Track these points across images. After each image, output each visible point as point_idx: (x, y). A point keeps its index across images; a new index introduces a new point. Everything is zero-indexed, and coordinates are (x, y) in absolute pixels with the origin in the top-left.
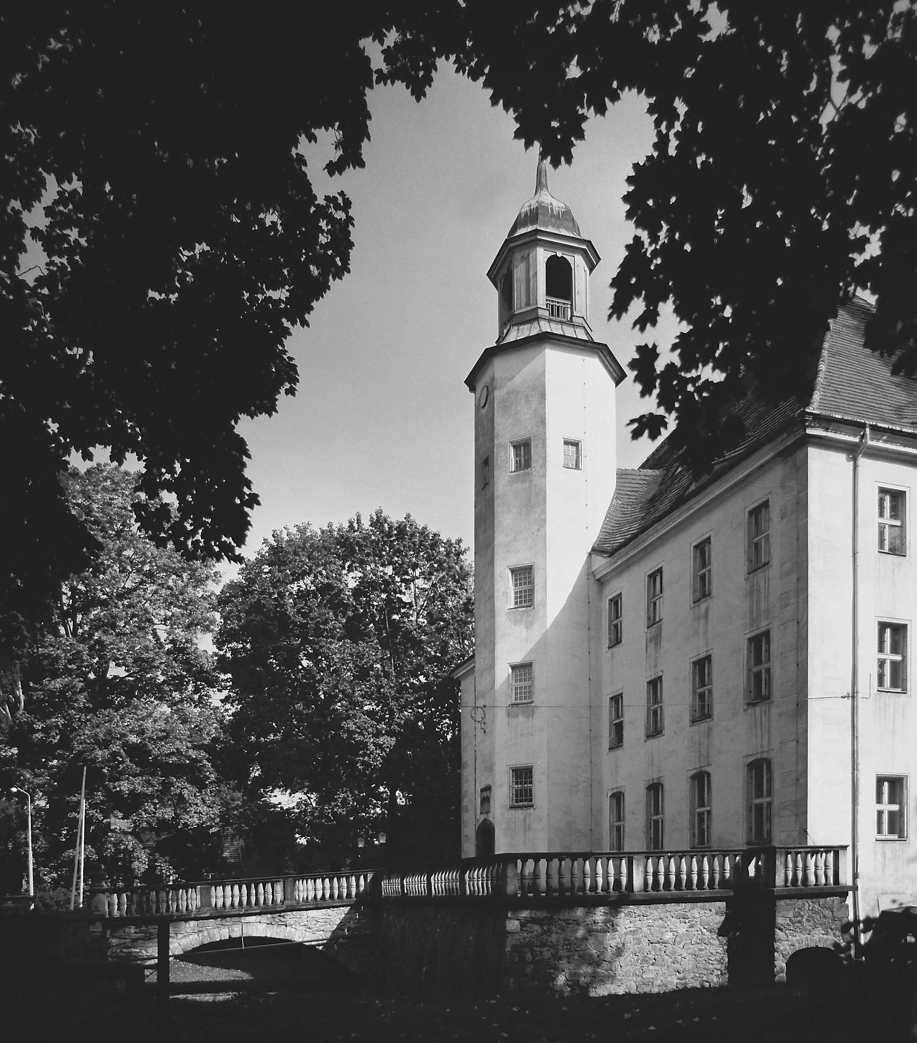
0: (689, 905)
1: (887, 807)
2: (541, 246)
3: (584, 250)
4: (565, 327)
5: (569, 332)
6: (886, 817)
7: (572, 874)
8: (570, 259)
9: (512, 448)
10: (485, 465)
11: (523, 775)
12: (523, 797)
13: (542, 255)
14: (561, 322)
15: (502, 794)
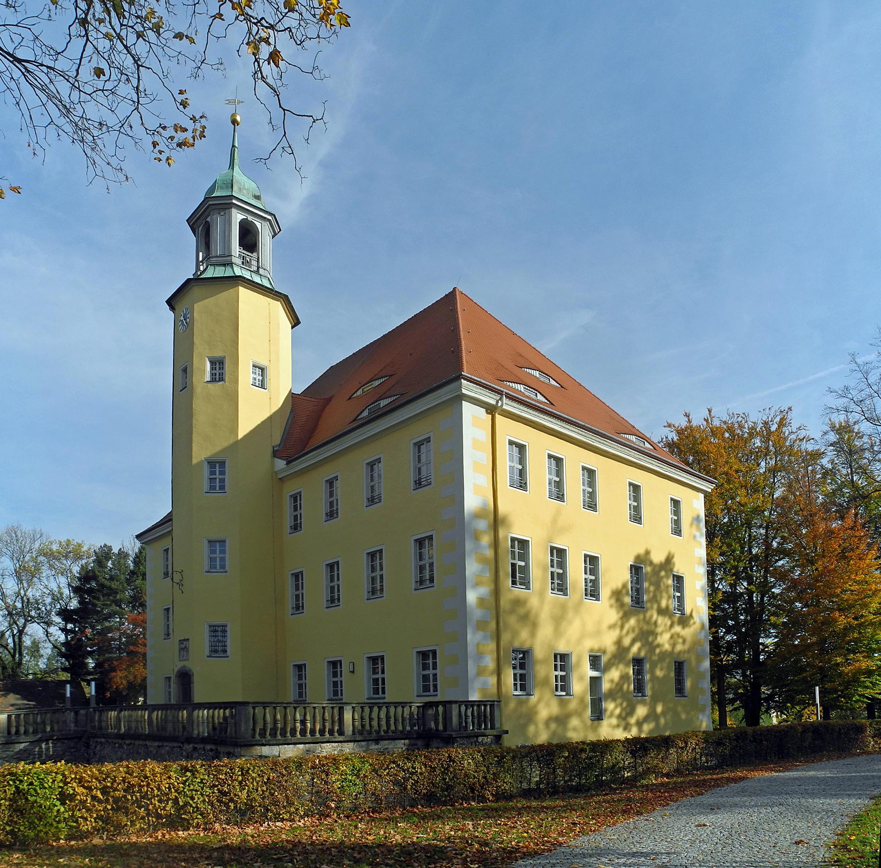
1: (431, 672)
3: (269, 220)
5: (257, 279)
8: (258, 225)
9: (208, 365)
10: (183, 374)
11: (218, 632)
12: (218, 649)
13: (237, 217)
15: (201, 642)
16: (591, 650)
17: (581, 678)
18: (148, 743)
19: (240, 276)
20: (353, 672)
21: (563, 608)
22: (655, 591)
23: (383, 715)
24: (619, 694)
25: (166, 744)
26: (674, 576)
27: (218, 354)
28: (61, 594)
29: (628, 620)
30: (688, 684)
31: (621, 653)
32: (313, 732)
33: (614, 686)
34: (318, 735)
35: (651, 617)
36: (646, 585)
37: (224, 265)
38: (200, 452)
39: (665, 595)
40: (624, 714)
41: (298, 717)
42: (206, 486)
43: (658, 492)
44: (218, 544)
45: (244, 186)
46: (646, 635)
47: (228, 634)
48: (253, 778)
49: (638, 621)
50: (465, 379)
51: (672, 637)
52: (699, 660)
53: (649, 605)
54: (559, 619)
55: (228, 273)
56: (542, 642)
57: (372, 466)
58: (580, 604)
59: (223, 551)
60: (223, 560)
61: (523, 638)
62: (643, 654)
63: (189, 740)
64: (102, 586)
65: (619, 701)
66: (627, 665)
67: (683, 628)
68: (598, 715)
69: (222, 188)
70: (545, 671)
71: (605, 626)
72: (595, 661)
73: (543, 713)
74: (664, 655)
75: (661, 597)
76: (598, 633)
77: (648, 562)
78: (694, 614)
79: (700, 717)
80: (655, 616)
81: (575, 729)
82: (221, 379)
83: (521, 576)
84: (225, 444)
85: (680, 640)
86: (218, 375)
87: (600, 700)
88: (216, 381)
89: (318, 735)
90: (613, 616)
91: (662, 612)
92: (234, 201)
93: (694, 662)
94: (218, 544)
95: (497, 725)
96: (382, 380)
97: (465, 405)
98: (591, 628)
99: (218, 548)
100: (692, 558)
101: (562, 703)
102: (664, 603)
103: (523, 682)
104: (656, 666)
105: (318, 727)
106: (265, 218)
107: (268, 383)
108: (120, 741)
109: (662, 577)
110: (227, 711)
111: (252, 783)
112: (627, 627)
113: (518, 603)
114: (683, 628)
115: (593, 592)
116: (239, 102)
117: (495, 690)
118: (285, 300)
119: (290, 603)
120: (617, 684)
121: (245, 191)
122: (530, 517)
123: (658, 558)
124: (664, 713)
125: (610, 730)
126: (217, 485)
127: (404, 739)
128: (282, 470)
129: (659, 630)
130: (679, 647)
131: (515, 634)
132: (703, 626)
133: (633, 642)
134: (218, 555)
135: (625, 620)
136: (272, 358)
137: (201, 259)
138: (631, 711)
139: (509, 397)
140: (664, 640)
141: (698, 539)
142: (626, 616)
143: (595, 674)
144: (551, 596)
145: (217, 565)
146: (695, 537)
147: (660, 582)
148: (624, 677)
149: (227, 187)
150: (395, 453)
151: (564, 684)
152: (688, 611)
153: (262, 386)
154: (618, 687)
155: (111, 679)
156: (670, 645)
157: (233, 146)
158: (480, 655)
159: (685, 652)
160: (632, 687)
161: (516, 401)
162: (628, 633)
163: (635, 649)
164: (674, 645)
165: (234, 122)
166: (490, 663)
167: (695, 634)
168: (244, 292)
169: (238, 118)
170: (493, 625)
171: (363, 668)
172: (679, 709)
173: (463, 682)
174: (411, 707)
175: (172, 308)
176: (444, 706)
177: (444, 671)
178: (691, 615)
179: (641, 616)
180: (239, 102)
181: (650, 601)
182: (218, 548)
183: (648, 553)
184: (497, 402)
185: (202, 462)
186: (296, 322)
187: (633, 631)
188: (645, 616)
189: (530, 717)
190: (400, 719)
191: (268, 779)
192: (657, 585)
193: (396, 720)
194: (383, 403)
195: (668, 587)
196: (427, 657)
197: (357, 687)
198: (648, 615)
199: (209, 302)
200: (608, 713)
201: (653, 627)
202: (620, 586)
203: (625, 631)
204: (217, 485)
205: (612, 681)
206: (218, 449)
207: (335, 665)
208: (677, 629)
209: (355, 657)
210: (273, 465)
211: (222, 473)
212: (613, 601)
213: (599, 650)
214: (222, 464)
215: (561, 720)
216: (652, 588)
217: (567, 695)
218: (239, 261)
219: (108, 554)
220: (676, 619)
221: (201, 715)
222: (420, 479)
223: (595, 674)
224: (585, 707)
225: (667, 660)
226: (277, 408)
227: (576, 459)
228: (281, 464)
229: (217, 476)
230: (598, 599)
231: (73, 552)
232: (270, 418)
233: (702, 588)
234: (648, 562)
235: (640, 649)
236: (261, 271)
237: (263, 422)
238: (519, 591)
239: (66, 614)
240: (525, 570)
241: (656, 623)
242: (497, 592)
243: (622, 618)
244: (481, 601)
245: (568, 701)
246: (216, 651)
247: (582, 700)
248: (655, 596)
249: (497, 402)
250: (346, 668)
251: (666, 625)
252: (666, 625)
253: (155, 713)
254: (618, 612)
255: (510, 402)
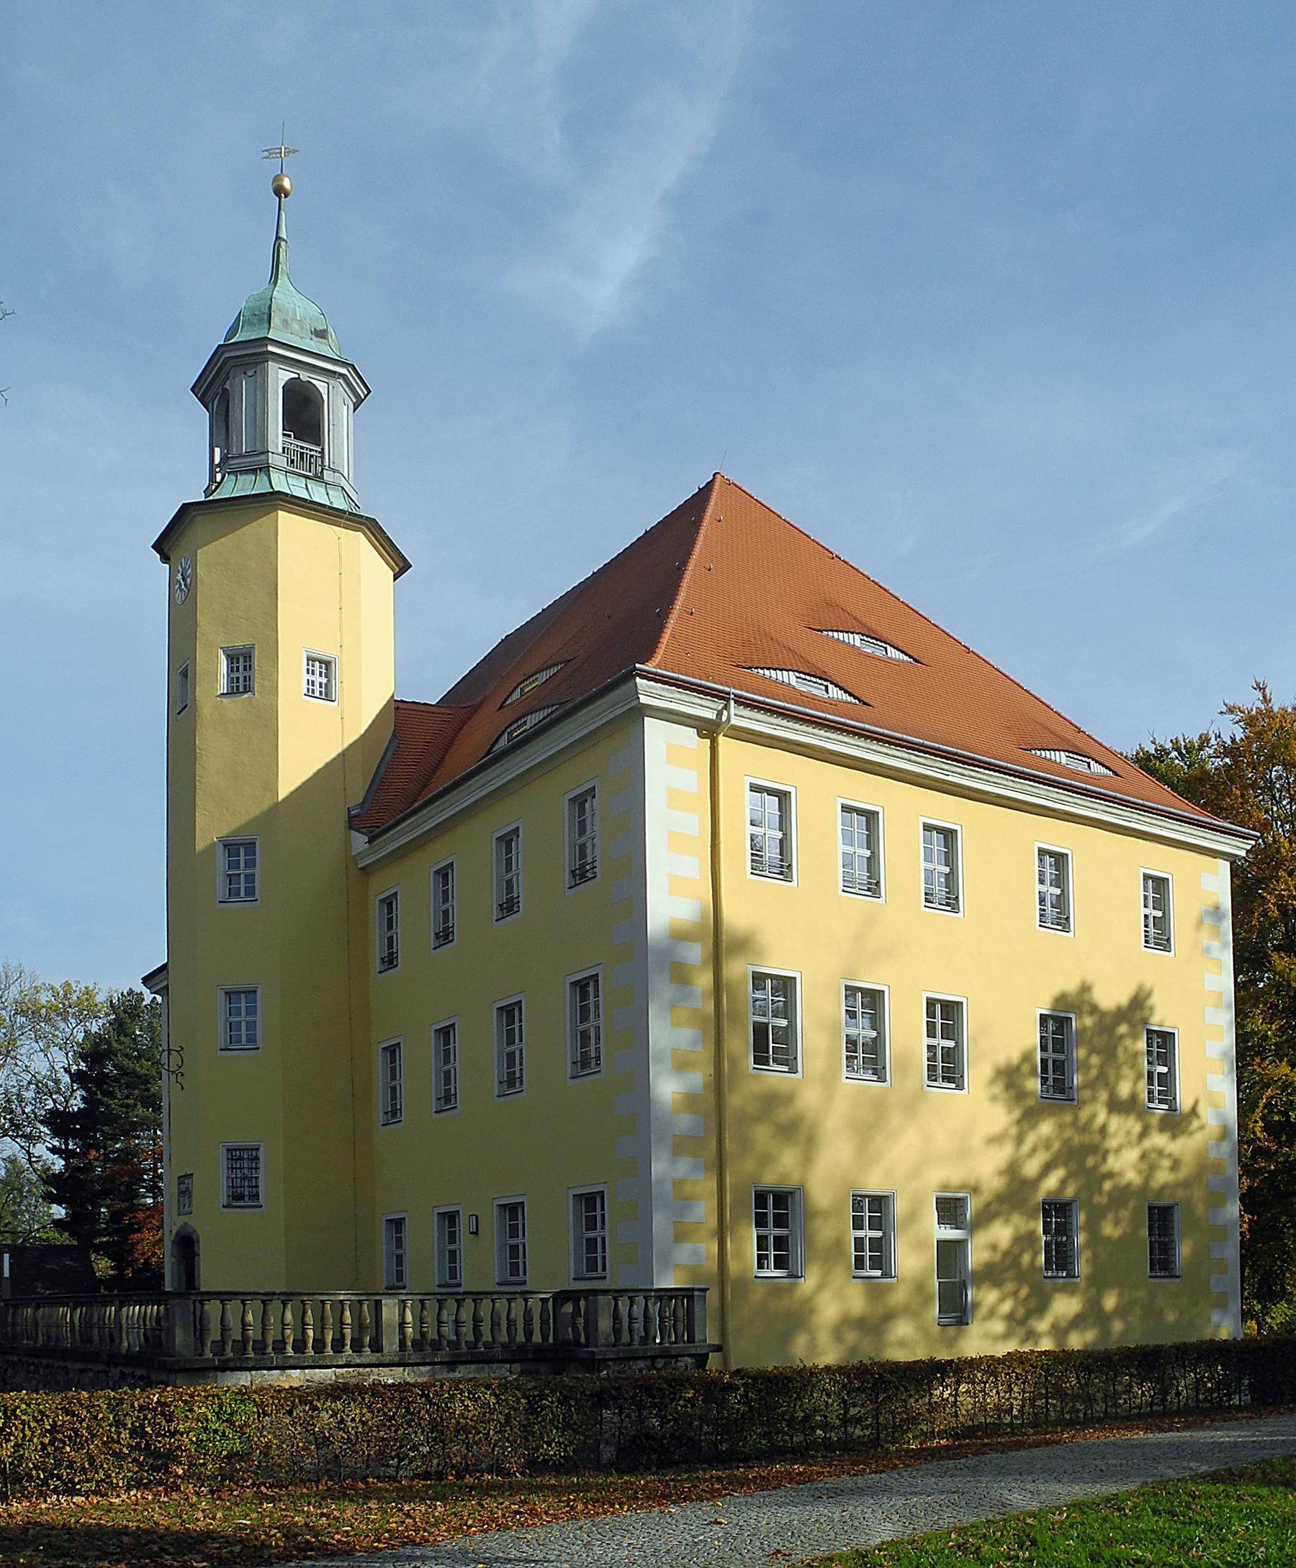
0: (386, 1370)
2: (273, 360)
3: (341, 375)
4: (311, 484)
5: (318, 494)
6: (600, 1268)
7: (439, 1322)
8: (322, 387)
10: (182, 676)
11: (243, 1159)
12: (242, 1193)
13: (279, 376)
14: (306, 477)
15: (213, 1181)
16: (945, 1187)
17: (920, 1245)
18: (69, 1364)
19: (279, 492)
20: (476, 1233)
21: (879, 1107)
22: (1102, 1067)
23: (466, 1315)
24: (1011, 1274)
25: (90, 1366)
26: (1149, 1032)
27: (240, 642)
28: (57, 1082)
29: (1034, 1125)
30: (1184, 1250)
31: (1015, 1192)
32: (319, 1345)
33: (998, 1257)
34: (310, 1351)
35: (1093, 1117)
36: (1081, 1053)
37: (254, 471)
38: (210, 828)
39: (1126, 1071)
40: (1021, 1312)
41: (289, 1317)
42: (221, 890)
43: (1110, 866)
44: (243, 996)
45: (296, 312)
46: (1081, 1155)
47: (261, 1164)
48: (23, 1422)
49: (1061, 1127)
50: (643, 677)
51: (1143, 1156)
52: (1216, 1200)
53: (1086, 1094)
54: (868, 1129)
55: (261, 487)
56: (826, 1176)
57: (509, 844)
58: (919, 1096)
59: (252, 1011)
60: (251, 1026)
61: (784, 1167)
62: (1070, 1192)
63: (113, 1359)
64: (124, 1072)
65: (1010, 1287)
66: (1031, 1216)
67: (1174, 1137)
68: (956, 1311)
69: (251, 323)
70: (832, 1226)
71: (977, 1140)
72: (949, 1209)
73: (829, 1310)
74: (1122, 1195)
75: (1118, 1077)
76: (963, 1153)
77: (1086, 1008)
78: (1201, 1109)
79: (1215, 1317)
80: (1102, 1116)
81: (902, 1344)
82: (248, 689)
83: (773, 1045)
84: (255, 811)
85: (1166, 1163)
86: (241, 684)
87: (963, 1286)
88: (238, 692)
89: (310, 1351)
90: (999, 1117)
91: (1115, 1106)
92: (270, 348)
93: (1200, 1209)
94: (243, 996)
95: (698, 1337)
96: (552, 671)
97: (652, 726)
98: (944, 1145)
99: (243, 1005)
100: (1198, 999)
101: (875, 1292)
102: (1124, 1090)
103: (781, 1252)
104: (1104, 1216)
105: (329, 1337)
106: (335, 372)
107: (336, 690)
108: (36, 1361)
109: (1122, 1037)
110: (162, 1308)
111: (23, 1431)
112: (1031, 1139)
113: (773, 1101)
114: (1174, 1137)
115: (947, 1068)
116: (288, 152)
117: (713, 1265)
118: (372, 528)
119: (380, 1103)
120: (1006, 1254)
121: (295, 326)
122: (804, 934)
123: (1110, 996)
124: (1121, 1311)
125: (984, 1339)
126: (240, 886)
127: (511, 1362)
128: (362, 854)
129: (1112, 1143)
130: (1163, 1176)
131: (767, 1160)
132: (1225, 1133)
133: (1047, 1168)
134: (243, 1018)
135: (1025, 1125)
136: (352, 641)
137: (217, 461)
138: (1039, 1305)
139: (741, 701)
140: (1125, 1163)
141: (1215, 953)
142: (1029, 1117)
143: (950, 1234)
144: (853, 1086)
145: (239, 1037)
146: (1207, 950)
147: (1115, 1049)
148: (1023, 1241)
149: (260, 321)
150: (540, 816)
151: (877, 1255)
152: (1184, 1099)
153: (327, 695)
154: (1008, 1261)
155: (133, 1245)
156: (1140, 1172)
157: (278, 238)
158: (683, 1202)
159: (1177, 1185)
160: (1042, 1258)
161: (759, 709)
162: (1034, 1150)
163: (1052, 1182)
164: (1152, 1170)
165: (279, 191)
166: (705, 1212)
167: (1202, 1154)
168: (286, 520)
169: (287, 183)
170: (713, 1143)
171: (492, 1225)
172: (1161, 1301)
173: (642, 1251)
174: (526, 1300)
175: (165, 558)
176: (586, 1299)
177: (614, 1231)
178: (1194, 1112)
179: (1068, 1118)
180: (288, 152)
181: (1092, 1085)
182: (243, 1005)
183: (1085, 989)
184: (720, 714)
185: (213, 845)
186: (401, 566)
187: (1048, 1147)
188: (1076, 1118)
189: (800, 1318)
190: (504, 1323)
191: (54, 1425)
192: (1109, 1053)
193: (544, 1322)
194: (532, 720)
195: (1136, 1055)
196: (590, 1203)
197: (424, 1263)
198: (1084, 1114)
199: (224, 545)
200: (983, 1310)
201: (1097, 1138)
202: (1015, 1057)
203: (1026, 1148)
204: (240, 886)
205: (994, 1247)
206: (242, 820)
207: (451, 1218)
208: (1159, 1140)
209: (480, 1204)
210: (347, 841)
211: (251, 864)
212: (998, 1089)
213: (963, 1187)
214: (250, 847)
215: (873, 1325)
216: (1095, 1060)
217: (884, 1275)
218: (280, 461)
219: (135, 1007)
220: (1154, 1121)
221: (149, 1310)
222: (582, 866)
223: (950, 1234)
224: (929, 1299)
225: (1132, 1204)
226: (356, 736)
227: (906, 811)
228: (359, 841)
229: (242, 870)
230: (960, 1087)
231: (71, 1005)
232: (343, 754)
233: (1224, 1054)
234: (1086, 1008)
235: (1063, 1183)
236: (328, 476)
237: (327, 764)
238: (775, 1076)
239: (59, 1122)
240: (787, 1036)
241: (1103, 1130)
242: (719, 1084)
243: (1019, 1122)
244: (690, 1101)
245: (889, 1288)
246: (241, 1197)
247: (919, 1287)
248: (1102, 1075)
249: (720, 714)
250: (463, 1226)
251: (1128, 1133)
252: (1128, 1133)
253: (125, 1309)
254: (1010, 1111)
255: (747, 712)
